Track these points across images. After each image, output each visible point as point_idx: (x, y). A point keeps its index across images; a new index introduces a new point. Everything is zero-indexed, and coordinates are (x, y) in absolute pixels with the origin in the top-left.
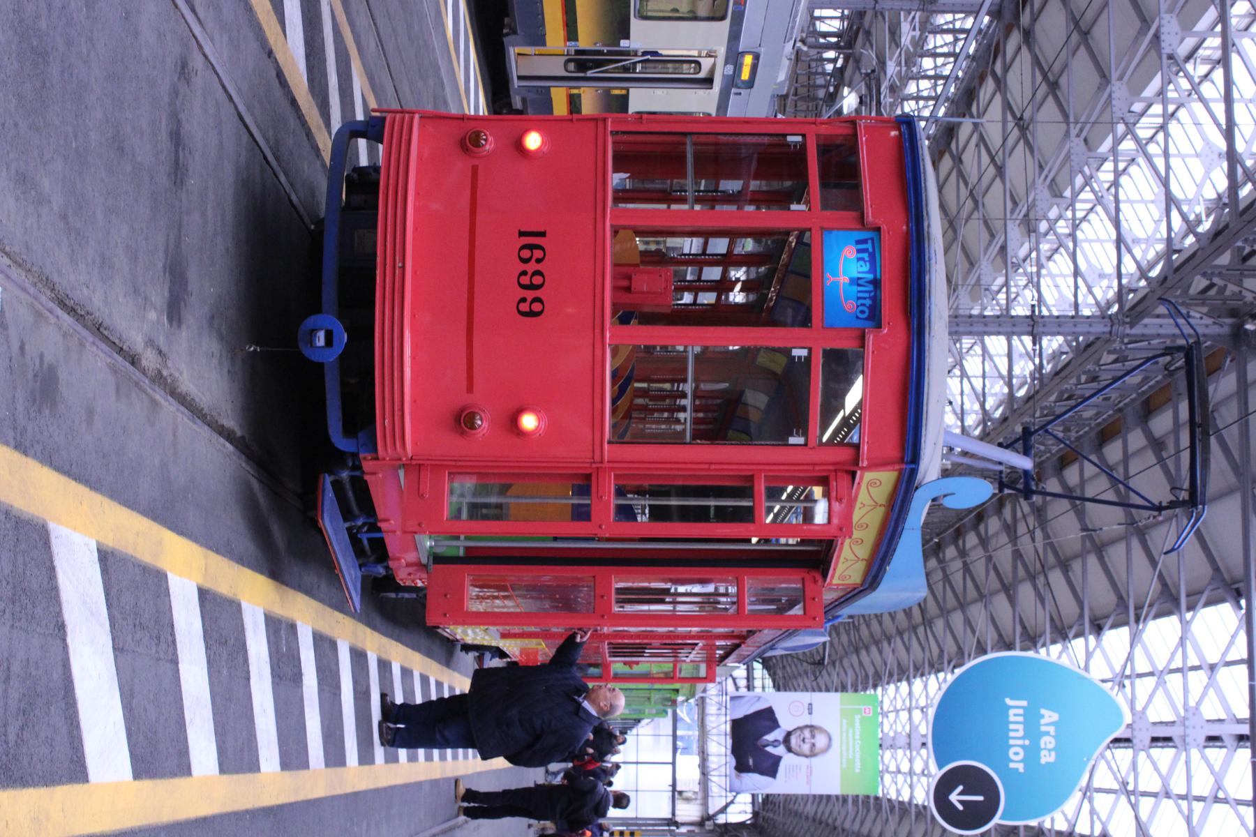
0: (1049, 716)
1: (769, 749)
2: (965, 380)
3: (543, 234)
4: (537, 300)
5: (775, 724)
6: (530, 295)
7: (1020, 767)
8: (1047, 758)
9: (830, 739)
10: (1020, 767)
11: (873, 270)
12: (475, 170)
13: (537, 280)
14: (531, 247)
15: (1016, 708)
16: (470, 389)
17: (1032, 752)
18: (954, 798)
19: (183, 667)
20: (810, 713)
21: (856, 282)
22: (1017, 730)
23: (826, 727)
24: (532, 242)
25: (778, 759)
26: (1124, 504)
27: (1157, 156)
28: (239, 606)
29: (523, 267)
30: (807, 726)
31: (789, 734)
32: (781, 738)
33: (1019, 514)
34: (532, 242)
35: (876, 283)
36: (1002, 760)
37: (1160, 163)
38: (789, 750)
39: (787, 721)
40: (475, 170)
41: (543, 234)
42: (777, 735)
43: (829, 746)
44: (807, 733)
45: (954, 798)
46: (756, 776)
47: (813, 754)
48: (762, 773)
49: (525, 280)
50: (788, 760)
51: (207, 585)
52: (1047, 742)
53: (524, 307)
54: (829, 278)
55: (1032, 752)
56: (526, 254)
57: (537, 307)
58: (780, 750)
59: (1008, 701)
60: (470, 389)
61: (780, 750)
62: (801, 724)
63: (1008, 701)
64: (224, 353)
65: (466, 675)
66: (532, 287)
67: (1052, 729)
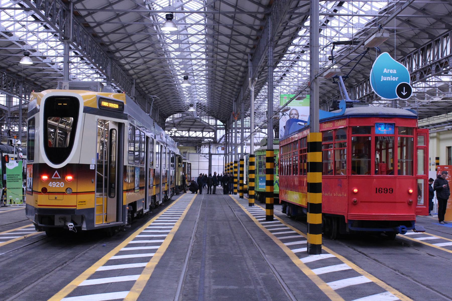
0: (385, 71)
2: (36, 42)
3: (376, 188)
4: (389, 189)
6: (388, 191)
7: (397, 78)
8: (395, 72)
10: (397, 78)
11: (383, 124)
12: (361, 202)
13: (386, 189)
14: (379, 191)
15: (383, 79)
16: (405, 202)
17: (394, 75)
18: (404, 94)
21: (385, 128)
22: (388, 79)
24: (378, 190)
28: (140, 274)
29: (383, 192)
34: (378, 190)
35: (385, 124)
36: (396, 82)
40: (361, 202)
41: (376, 188)
43: (295, 109)
45: (404, 94)
47: (298, 114)
49: (386, 192)
51: (136, 283)
52: (391, 71)
53: (391, 192)
54: (385, 133)
55: (394, 75)
56: (380, 192)
57: (391, 190)
59: (382, 80)
60: (405, 202)
63: (382, 80)
64: (360, 249)
66: (387, 190)
67: (388, 70)
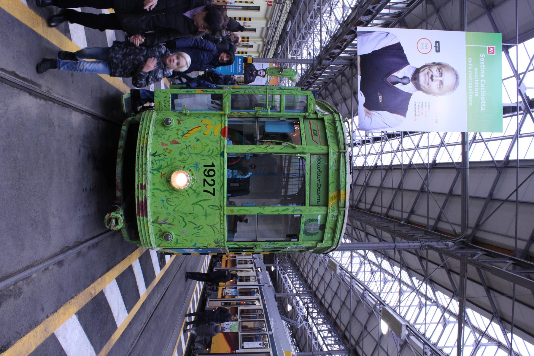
1: (399, 86)
5: (404, 62)
9: (457, 78)
19: (31, 334)
20: (438, 51)
23: (452, 65)
25: (409, 95)
26: (491, 198)
27: (436, 76)
30: (434, 64)
31: (417, 71)
32: (410, 76)
33: (362, 270)
37: (401, 146)
38: (418, 87)
39: (415, 58)
42: (405, 72)
43: (456, 84)
44: (435, 70)
46: (385, 114)
48: (392, 111)
50: (417, 98)
58: (409, 88)
61: (409, 88)
62: (429, 62)
65: (105, 33)
